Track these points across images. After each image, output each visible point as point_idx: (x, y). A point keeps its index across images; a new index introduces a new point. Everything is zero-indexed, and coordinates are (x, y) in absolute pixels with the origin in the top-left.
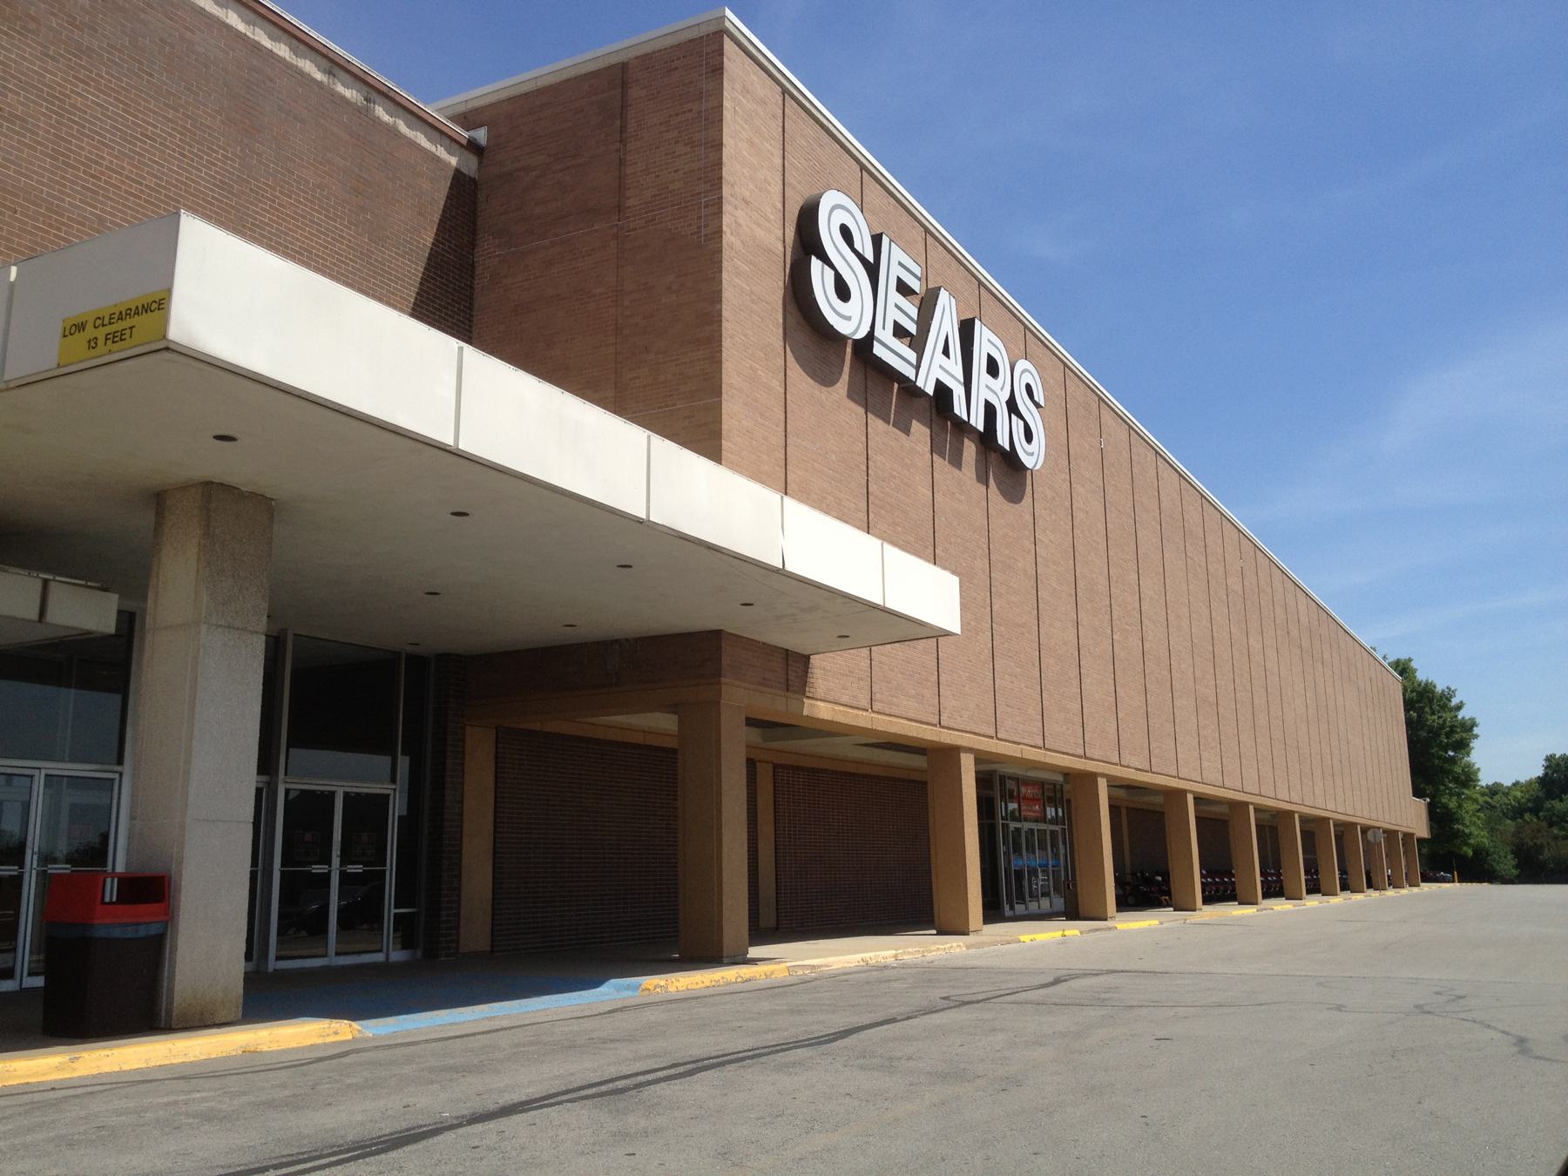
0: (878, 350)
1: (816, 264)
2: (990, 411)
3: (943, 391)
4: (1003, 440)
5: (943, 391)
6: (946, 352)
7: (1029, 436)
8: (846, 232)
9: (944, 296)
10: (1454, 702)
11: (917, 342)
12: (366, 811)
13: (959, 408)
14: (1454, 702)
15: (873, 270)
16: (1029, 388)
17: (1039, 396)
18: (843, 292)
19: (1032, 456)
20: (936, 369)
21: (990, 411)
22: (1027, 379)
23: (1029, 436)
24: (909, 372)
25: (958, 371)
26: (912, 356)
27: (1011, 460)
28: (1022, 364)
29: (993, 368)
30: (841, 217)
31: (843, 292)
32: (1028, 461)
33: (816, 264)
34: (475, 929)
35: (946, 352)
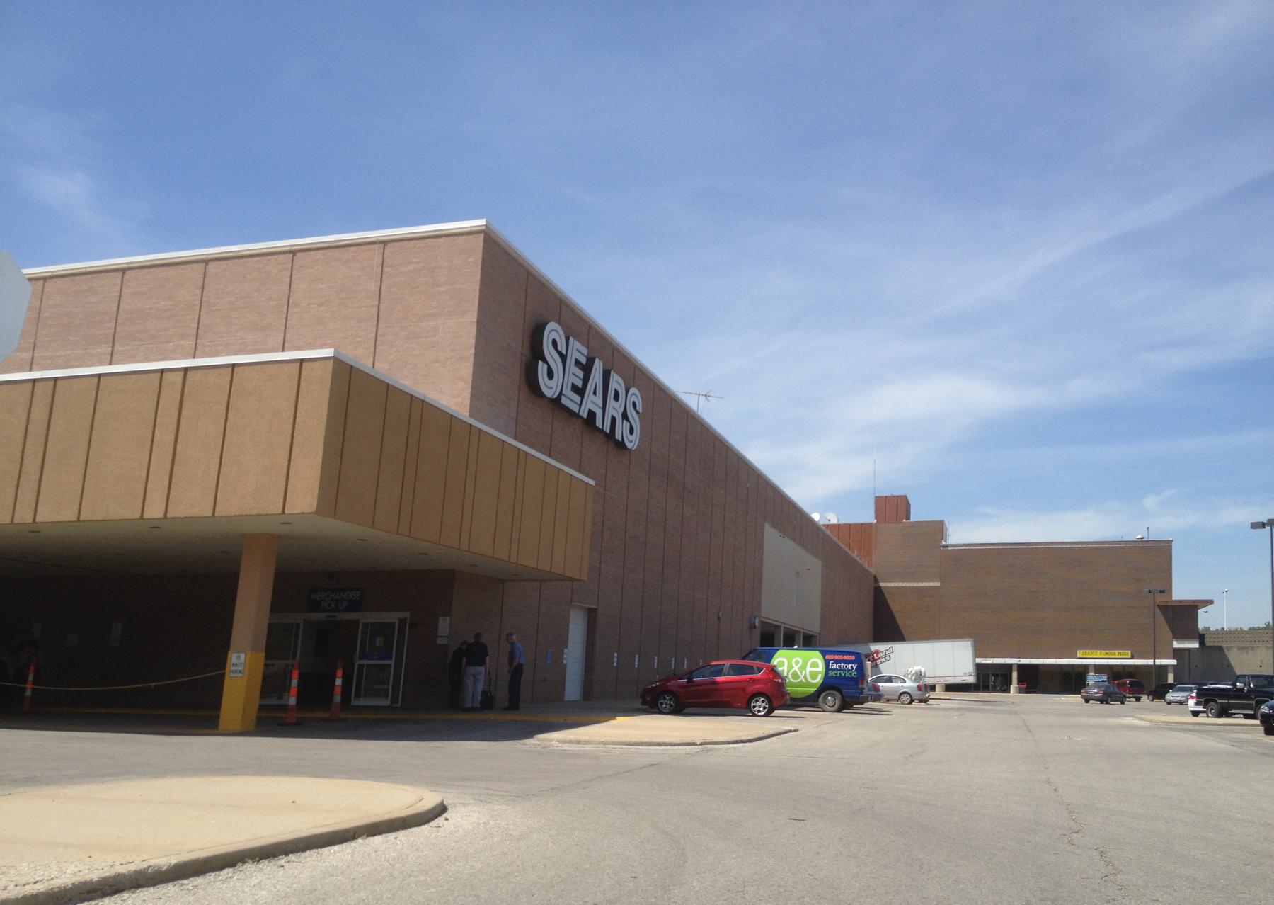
0: (564, 401)
1: (540, 363)
2: (613, 419)
3: (592, 414)
4: (618, 437)
5: (592, 414)
6: (595, 393)
7: (631, 431)
8: (554, 343)
9: (597, 361)
10: (441, 369)
11: (580, 391)
12: (358, 695)
13: (599, 423)
14: (441, 369)
15: (563, 358)
16: (634, 405)
17: (639, 408)
18: (550, 375)
19: (632, 442)
20: (592, 402)
21: (613, 419)
22: (634, 398)
23: (631, 431)
24: (575, 408)
25: (600, 402)
26: (578, 399)
27: (621, 445)
28: (633, 390)
29: (616, 397)
30: (554, 335)
31: (550, 375)
32: (629, 445)
33: (540, 363)
34: (572, 690)
35: (595, 393)
